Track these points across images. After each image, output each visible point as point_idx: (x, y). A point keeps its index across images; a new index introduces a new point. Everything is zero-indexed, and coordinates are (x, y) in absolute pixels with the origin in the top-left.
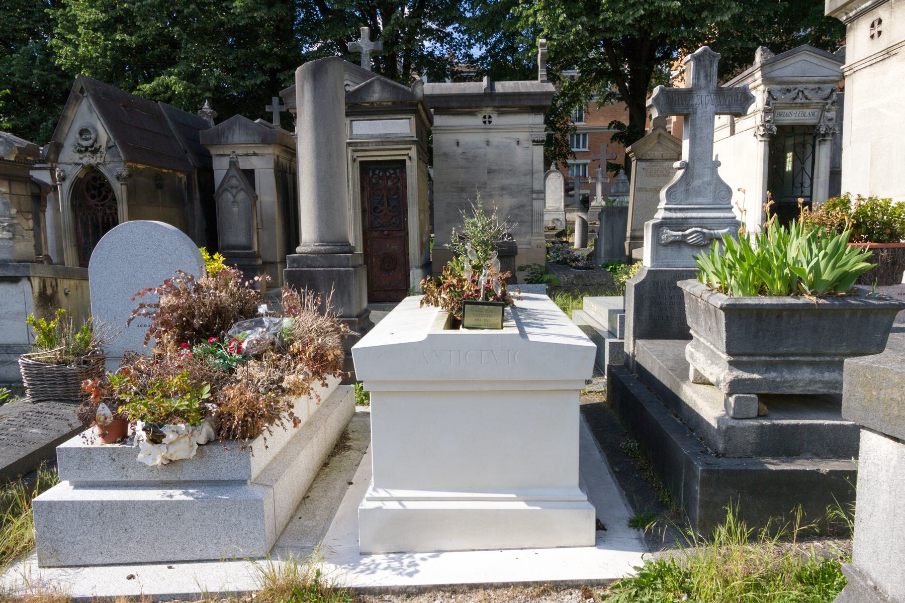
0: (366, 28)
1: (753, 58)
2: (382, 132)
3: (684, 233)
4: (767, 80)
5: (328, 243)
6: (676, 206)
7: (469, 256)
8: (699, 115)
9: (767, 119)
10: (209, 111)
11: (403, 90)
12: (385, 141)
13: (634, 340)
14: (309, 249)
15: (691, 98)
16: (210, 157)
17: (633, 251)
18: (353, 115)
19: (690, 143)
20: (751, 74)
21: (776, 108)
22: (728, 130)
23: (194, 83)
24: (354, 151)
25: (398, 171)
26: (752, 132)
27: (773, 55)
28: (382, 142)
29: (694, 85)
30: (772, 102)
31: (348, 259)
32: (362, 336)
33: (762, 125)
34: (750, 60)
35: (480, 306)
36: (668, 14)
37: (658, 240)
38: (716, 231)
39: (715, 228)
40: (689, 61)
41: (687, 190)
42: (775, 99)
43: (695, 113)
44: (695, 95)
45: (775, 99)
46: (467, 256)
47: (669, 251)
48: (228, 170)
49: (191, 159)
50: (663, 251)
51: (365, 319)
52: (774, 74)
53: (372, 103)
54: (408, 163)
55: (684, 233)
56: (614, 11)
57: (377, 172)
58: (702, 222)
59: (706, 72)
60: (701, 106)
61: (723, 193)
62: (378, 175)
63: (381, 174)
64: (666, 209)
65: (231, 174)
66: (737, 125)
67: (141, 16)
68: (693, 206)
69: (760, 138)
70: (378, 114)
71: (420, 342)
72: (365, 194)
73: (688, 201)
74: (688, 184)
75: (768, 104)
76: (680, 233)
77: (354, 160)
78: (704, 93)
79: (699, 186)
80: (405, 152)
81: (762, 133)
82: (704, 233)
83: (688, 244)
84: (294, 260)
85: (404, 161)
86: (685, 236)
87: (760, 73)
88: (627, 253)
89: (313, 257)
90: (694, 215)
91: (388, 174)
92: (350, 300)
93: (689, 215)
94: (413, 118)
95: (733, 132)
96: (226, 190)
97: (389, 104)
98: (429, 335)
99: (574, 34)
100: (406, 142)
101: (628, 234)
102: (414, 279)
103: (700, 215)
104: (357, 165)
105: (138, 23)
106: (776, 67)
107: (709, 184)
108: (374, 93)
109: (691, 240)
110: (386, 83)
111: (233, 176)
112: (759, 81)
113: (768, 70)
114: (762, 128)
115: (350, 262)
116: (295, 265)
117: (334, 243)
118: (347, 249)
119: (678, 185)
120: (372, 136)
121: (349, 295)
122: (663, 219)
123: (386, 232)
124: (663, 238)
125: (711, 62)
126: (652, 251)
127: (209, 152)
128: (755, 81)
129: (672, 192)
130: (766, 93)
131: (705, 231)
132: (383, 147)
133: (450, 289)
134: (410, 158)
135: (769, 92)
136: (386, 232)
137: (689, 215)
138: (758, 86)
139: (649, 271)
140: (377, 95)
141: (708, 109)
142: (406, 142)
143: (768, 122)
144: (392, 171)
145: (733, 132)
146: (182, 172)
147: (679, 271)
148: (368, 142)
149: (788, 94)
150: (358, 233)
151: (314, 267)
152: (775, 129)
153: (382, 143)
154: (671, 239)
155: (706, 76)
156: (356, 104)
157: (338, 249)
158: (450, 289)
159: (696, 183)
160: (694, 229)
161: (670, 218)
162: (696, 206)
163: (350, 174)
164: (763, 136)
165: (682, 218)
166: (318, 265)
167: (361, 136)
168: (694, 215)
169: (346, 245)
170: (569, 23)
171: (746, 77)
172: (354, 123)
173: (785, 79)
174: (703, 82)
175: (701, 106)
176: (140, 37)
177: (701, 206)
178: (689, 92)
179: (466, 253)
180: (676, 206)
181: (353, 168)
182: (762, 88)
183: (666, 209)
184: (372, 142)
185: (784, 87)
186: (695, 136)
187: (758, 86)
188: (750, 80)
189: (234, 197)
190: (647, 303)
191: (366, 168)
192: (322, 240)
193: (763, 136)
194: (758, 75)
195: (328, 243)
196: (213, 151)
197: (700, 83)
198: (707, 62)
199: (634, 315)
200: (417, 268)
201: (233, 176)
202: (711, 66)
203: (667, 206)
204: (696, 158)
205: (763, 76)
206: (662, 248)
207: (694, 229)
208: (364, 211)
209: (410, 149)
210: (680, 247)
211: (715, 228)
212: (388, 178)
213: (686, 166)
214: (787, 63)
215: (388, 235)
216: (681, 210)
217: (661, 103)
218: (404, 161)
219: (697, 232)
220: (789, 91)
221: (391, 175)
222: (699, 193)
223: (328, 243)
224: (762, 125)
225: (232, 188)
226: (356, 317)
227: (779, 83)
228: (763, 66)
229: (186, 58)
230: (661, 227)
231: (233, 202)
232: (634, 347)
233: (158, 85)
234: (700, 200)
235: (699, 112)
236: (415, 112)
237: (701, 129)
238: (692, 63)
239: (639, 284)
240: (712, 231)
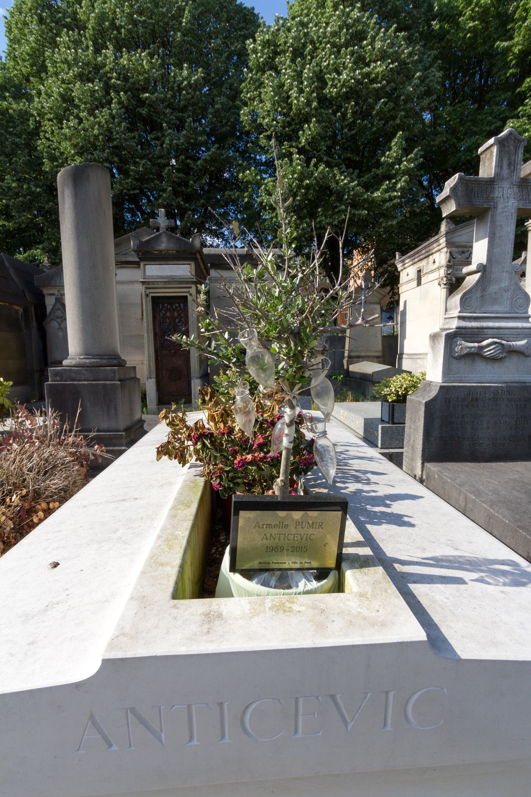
0: (163, 210)
1: (439, 229)
2: (169, 274)
3: (480, 344)
4: (449, 244)
5: (94, 356)
6: (471, 315)
7: (252, 370)
8: (500, 210)
9: (449, 272)
10: (48, 265)
11: (185, 241)
12: (171, 281)
13: (423, 464)
14: (74, 362)
15: (493, 190)
16: (43, 296)
17: (350, 366)
18: (146, 260)
19: (489, 242)
20: (437, 241)
21: (455, 265)
22: (415, 282)
23: (54, 255)
24: (147, 288)
25: (182, 305)
26: (437, 282)
27: (454, 226)
28: (169, 282)
29: (496, 174)
30: (452, 260)
31: (114, 372)
32: (116, 459)
33: (446, 277)
34: (437, 231)
35: (282, 514)
36: (359, 219)
37: (451, 352)
38: (514, 343)
39: (512, 339)
40: (491, 146)
41: (482, 296)
42: (454, 258)
43: (495, 207)
44: (497, 187)
45: (454, 258)
46: (243, 372)
47: (462, 365)
48: (54, 306)
49: (29, 297)
50: (455, 365)
51: (139, 429)
52: (454, 240)
53: (161, 251)
54: (190, 298)
55: (480, 344)
56: (326, 217)
57: (166, 305)
58: (498, 332)
59: (509, 159)
60: (502, 199)
61: (521, 301)
62: (167, 307)
63: (169, 307)
64: (459, 318)
65: (56, 307)
66: (422, 279)
67: (15, 208)
68: (489, 315)
69: (443, 286)
70: (323, 507)
71: (77, 685)
72: (157, 322)
73: (483, 309)
74: (484, 290)
75: (449, 261)
76: (476, 345)
77: (147, 296)
78: (506, 184)
79: (496, 293)
80: (187, 290)
81: (445, 282)
82: (502, 345)
83: (485, 358)
84: (56, 374)
85: (186, 297)
86: (482, 348)
87: (444, 239)
88: (345, 367)
89: (77, 370)
90: (491, 324)
91: (174, 307)
92: (116, 414)
93: (485, 324)
94: (193, 264)
95: (419, 284)
96: (53, 319)
97: (174, 252)
98: (105, 662)
99: (301, 230)
100: (188, 282)
101: (346, 354)
102: (195, 386)
103: (497, 324)
104: (150, 299)
105: (13, 214)
106: (457, 234)
107: (506, 290)
108: (162, 243)
109: (487, 352)
110: (171, 236)
111: (58, 309)
112: (444, 245)
113: (450, 236)
114: (445, 279)
115: (117, 375)
116: (58, 378)
117: (100, 356)
118: (115, 362)
119: (473, 291)
120: (161, 277)
121: (116, 408)
122: (457, 328)
123: (173, 351)
124: (456, 350)
125: (516, 148)
126: (444, 364)
127: (42, 292)
128: (439, 245)
129: (467, 299)
130: (448, 254)
131: (504, 342)
132: (169, 286)
133: (204, 444)
134: (191, 294)
135: (450, 253)
136: (173, 351)
137: (485, 324)
138: (442, 249)
139: (441, 387)
140: (164, 244)
141: (510, 204)
142: (188, 282)
143: (449, 274)
144: (177, 305)
145: (419, 284)
146: (18, 305)
147: (473, 386)
148: (158, 282)
149: (463, 255)
150: (151, 352)
151: (79, 381)
152: (454, 279)
153: (169, 282)
154: (465, 352)
155: (509, 165)
156: (148, 252)
157: (105, 362)
158: (204, 444)
159: (493, 288)
160: (490, 340)
161: (465, 328)
162: (492, 315)
163: (144, 306)
164: (445, 284)
165: (478, 328)
166: (83, 378)
167: (152, 277)
168: (491, 324)
169: (115, 359)
170: (298, 222)
171: (432, 243)
172: (147, 266)
173: (461, 244)
174: (505, 171)
175: (502, 199)
176: (15, 223)
177: (498, 315)
178: (490, 182)
179: (241, 364)
180: (471, 315)
181: (146, 301)
182: (445, 250)
183: (459, 318)
184: (161, 282)
185: (460, 249)
186: (495, 234)
187: (442, 249)
188: (435, 245)
189: (60, 325)
190: (437, 422)
191: (156, 301)
192: (87, 353)
193: (445, 284)
194: (443, 241)
195: (94, 356)
196: (45, 291)
197: (503, 173)
198: (512, 148)
199: (424, 435)
200: (197, 378)
201: (58, 309)
202: (516, 152)
203: (461, 314)
204: (494, 260)
205: (446, 241)
206: (455, 361)
207: (490, 340)
208: (155, 335)
209: (190, 288)
210: (474, 360)
211: (512, 339)
212: (174, 310)
213: (482, 269)
214: (463, 232)
215: (175, 353)
216: (476, 319)
217: (459, 194)
218: (186, 297)
219: (495, 343)
220: (463, 252)
221: (176, 307)
222: (495, 301)
223: (94, 356)
224: (446, 277)
225: (58, 318)
226: (124, 431)
227: (458, 247)
228: (447, 234)
229: (48, 239)
230: (454, 338)
231: (59, 329)
232: (422, 471)
233: (29, 256)
234: (496, 308)
235: (500, 206)
236: (195, 259)
237: (501, 226)
238: (495, 149)
239: (430, 401)
240: (510, 343)
